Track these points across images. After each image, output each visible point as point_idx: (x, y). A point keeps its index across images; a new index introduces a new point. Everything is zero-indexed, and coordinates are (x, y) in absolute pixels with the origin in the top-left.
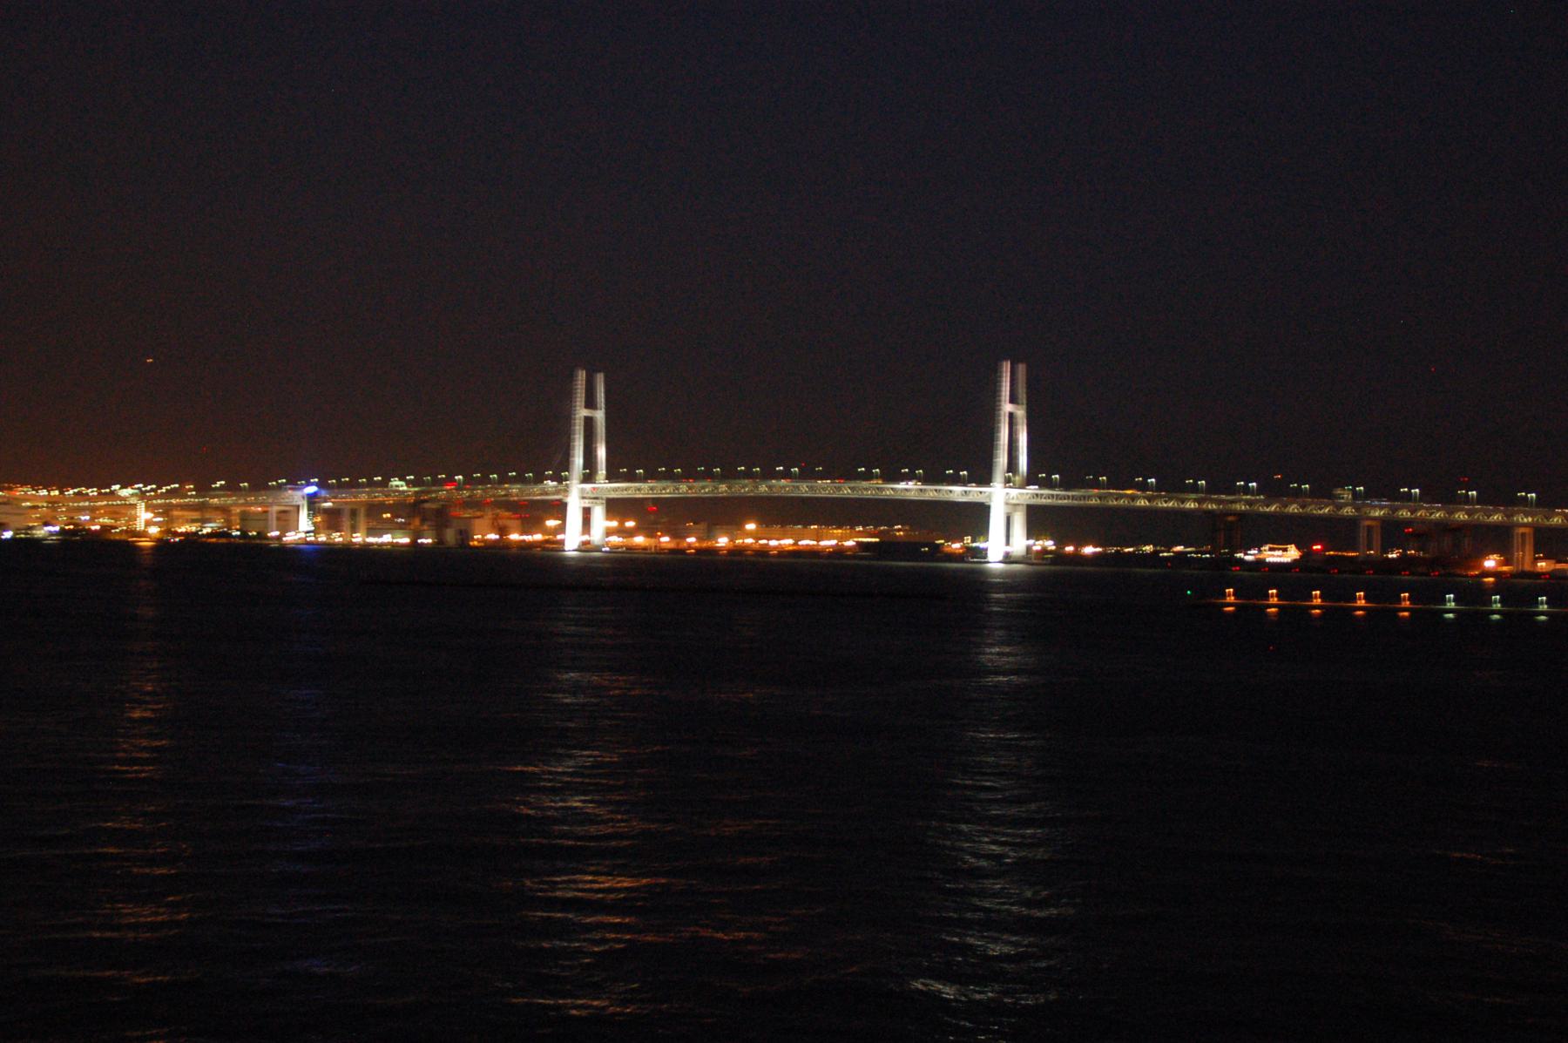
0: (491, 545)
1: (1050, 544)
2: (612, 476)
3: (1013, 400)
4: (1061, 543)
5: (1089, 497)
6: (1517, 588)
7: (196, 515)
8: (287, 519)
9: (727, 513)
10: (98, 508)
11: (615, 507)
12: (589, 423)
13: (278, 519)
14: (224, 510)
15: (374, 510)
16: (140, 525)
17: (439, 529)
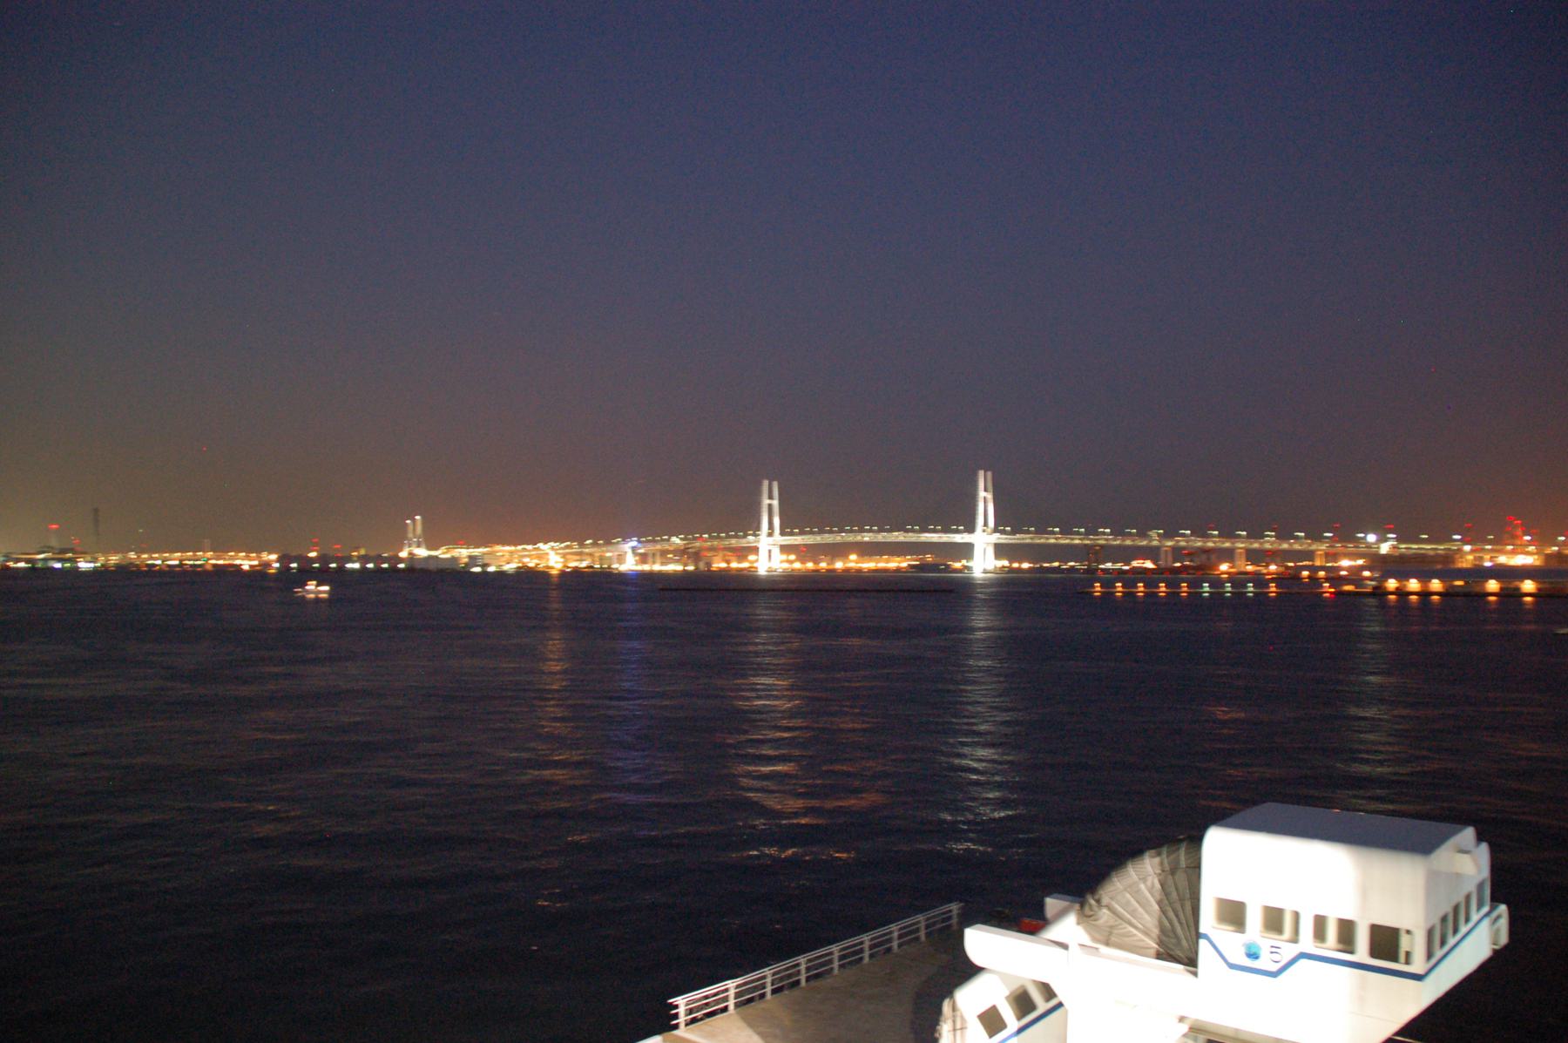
0: (721, 570)
1: (1006, 563)
2: (783, 533)
3: (986, 490)
4: (1011, 562)
5: (1026, 539)
6: (1238, 580)
7: (578, 558)
8: (621, 558)
9: (840, 550)
10: (533, 555)
11: (785, 549)
12: (770, 506)
13: (618, 559)
14: (591, 555)
15: (664, 553)
16: (551, 563)
17: (696, 563)
